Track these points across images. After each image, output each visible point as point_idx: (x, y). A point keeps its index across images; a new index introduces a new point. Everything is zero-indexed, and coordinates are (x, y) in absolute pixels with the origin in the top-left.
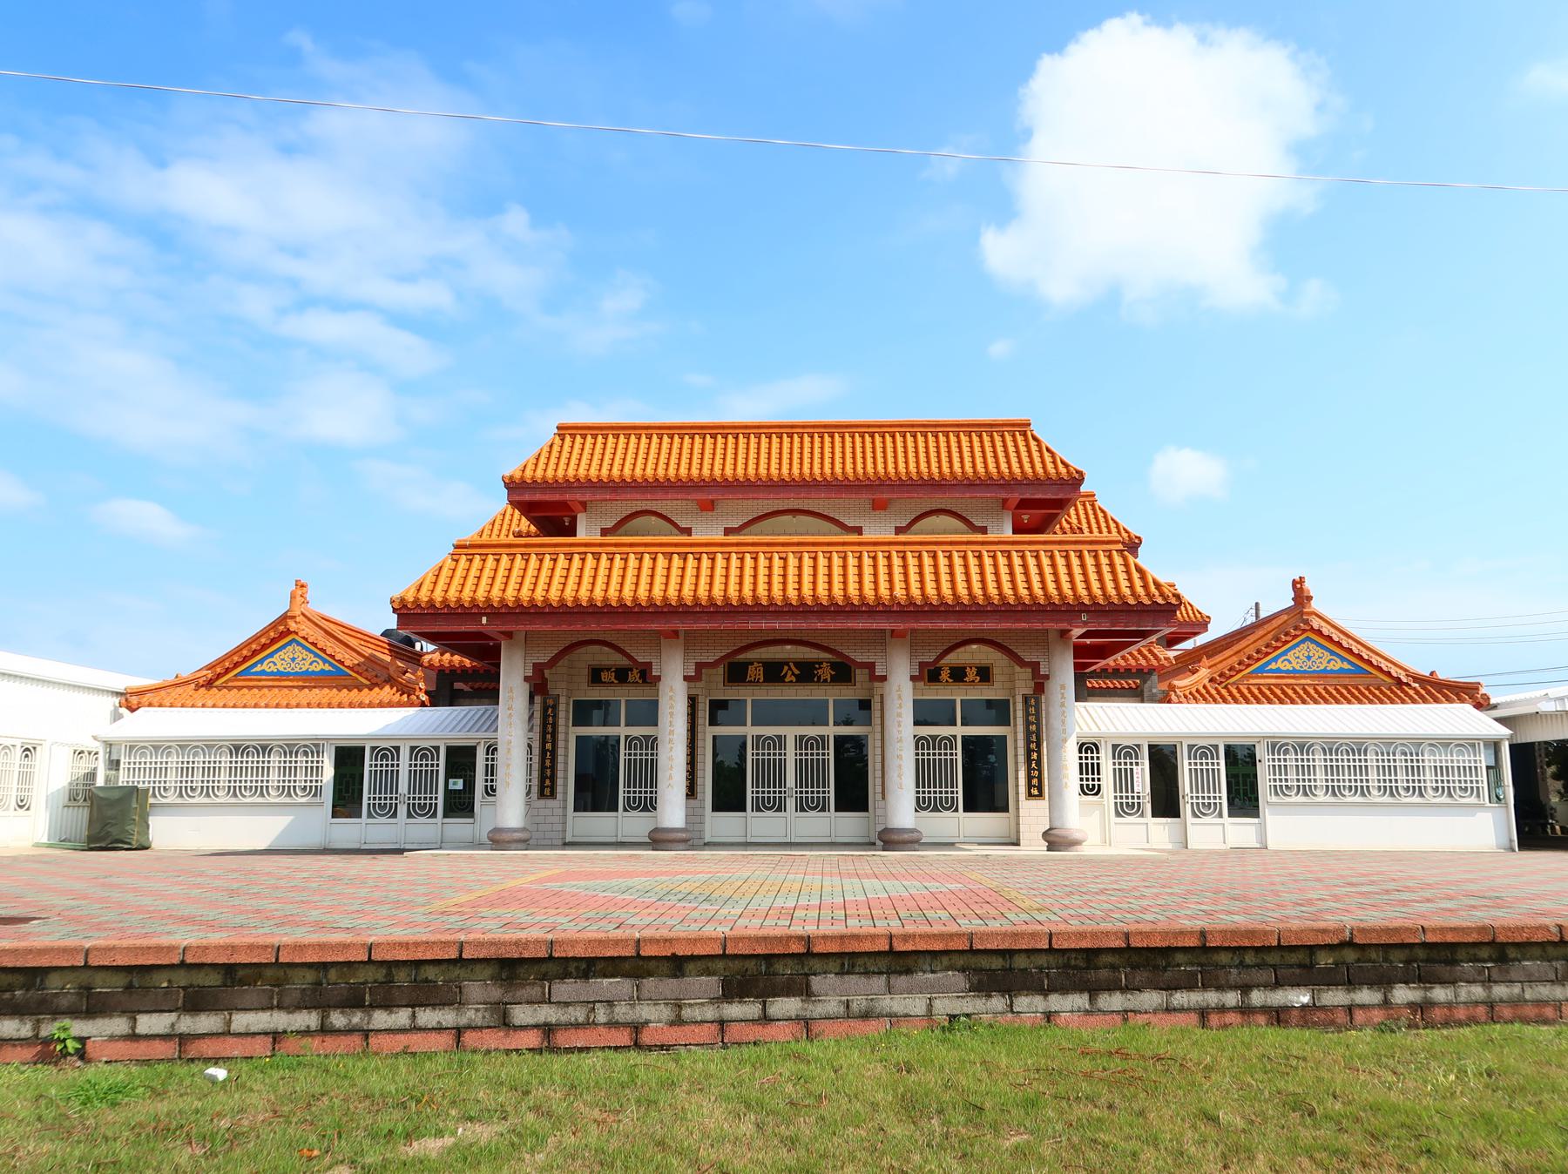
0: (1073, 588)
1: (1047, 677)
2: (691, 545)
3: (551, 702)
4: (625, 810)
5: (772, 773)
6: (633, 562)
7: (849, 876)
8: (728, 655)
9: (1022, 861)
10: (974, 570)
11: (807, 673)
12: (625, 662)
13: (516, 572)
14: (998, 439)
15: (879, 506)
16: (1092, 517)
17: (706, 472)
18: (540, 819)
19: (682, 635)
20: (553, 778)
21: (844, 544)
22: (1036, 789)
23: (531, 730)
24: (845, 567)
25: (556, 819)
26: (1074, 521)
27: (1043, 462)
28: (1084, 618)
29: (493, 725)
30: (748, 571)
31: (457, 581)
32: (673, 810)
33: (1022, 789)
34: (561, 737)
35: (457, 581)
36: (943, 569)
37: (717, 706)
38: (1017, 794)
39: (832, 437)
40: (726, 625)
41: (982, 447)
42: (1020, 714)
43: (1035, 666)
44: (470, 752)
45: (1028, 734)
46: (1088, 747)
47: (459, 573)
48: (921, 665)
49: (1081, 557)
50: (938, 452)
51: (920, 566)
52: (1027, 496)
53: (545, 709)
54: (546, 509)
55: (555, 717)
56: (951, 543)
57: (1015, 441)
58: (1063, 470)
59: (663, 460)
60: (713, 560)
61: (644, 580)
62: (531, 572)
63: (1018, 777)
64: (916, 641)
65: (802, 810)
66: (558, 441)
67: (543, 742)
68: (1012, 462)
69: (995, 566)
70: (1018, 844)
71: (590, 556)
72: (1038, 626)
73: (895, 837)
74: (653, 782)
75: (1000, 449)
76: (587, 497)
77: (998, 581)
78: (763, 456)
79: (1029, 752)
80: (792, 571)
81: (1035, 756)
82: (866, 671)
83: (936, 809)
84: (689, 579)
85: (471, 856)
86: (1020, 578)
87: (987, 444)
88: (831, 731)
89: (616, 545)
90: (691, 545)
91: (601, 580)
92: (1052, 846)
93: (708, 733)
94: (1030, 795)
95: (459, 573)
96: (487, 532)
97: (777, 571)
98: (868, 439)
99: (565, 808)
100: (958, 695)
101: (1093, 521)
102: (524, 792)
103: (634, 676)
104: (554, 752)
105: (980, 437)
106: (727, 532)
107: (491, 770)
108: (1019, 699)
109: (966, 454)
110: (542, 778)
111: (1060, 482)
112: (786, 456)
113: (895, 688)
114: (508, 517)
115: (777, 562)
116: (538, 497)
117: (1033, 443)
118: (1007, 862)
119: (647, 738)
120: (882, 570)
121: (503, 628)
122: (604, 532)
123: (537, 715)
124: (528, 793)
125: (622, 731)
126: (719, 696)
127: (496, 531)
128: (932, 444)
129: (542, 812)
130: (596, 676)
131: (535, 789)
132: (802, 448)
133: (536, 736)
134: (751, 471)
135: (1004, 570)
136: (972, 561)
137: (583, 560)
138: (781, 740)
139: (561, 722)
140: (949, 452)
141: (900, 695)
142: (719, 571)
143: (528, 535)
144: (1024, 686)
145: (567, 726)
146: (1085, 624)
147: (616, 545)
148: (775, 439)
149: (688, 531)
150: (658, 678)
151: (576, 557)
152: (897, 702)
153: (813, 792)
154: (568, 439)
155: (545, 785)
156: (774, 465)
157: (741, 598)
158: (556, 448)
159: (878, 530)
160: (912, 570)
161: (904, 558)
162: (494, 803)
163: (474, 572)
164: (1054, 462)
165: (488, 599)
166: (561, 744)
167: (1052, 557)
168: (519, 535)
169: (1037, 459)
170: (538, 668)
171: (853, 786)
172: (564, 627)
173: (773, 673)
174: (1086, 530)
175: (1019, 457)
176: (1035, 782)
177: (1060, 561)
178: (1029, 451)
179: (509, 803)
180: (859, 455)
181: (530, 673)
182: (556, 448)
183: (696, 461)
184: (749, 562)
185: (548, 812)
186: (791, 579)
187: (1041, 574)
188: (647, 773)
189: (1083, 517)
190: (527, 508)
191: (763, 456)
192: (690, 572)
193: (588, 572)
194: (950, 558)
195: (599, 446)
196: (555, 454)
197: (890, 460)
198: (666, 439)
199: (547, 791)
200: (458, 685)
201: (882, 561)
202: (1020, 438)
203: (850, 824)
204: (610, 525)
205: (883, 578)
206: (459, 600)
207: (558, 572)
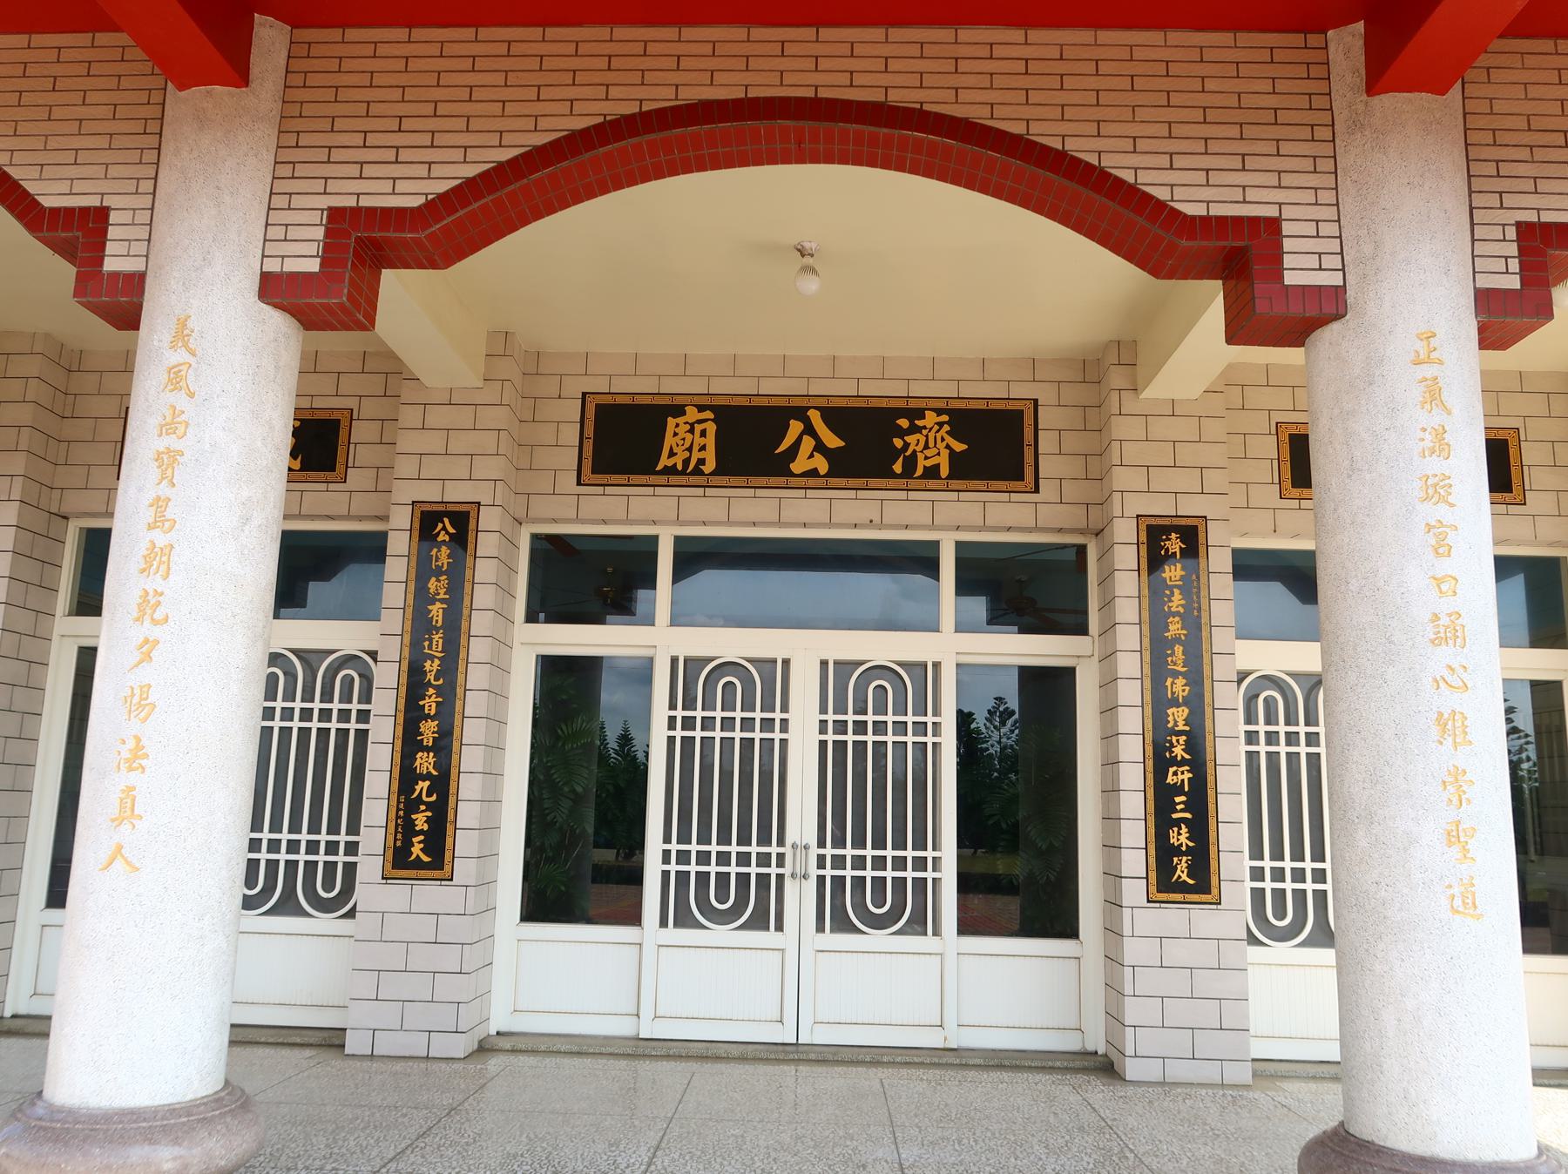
5: (738, 794)
20: (1162, 798)
33: (1135, 861)
34: (478, 649)
65: (842, 924)
108: (1125, 533)
138: (769, 680)
139: (483, 596)
145: (504, 616)
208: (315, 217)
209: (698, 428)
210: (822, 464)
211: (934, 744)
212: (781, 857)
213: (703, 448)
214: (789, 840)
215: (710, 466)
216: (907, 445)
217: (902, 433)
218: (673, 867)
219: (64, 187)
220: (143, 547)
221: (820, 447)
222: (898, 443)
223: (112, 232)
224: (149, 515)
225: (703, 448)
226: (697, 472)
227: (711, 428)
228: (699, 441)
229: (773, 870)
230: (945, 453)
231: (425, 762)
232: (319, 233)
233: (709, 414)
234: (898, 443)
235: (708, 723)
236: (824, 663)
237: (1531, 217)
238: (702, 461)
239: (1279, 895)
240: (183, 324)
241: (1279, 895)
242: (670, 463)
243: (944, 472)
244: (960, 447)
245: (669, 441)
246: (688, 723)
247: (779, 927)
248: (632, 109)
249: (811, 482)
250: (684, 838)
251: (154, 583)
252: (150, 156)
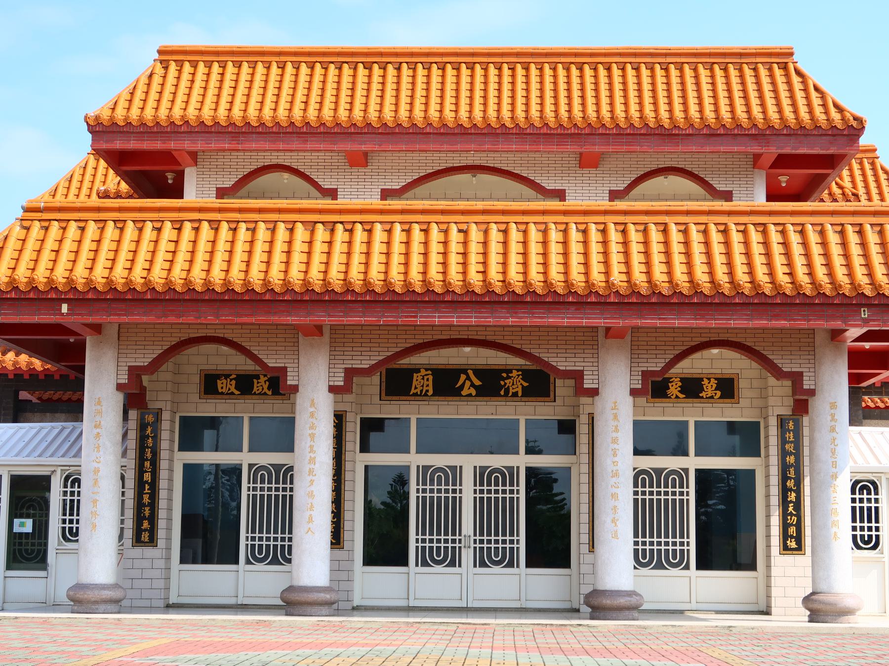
0: (851, 275)
1: (812, 393)
2: (341, 212)
3: (150, 418)
4: (248, 562)
5: (443, 517)
6: (262, 233)
7: (551, 651)
8: (388, 359)
9: (776, 635)
10: (717, 249)
11: (491, 384)
12: (247, 366)
13: (107, 245)
14: (748, 72)
15: (588, 162)
16: (871, 179)
17: (358, 114)
18: (136, 573)
19: (326, 331)
20: (153, 519)
21: (544, 213)
22: (793, 540)
23: (124, 454)
24: (545, 243)
25: (157, 573)
26: (847, 183)
27: (809, 105)
28: (865, 314)
29: (75, 447)
30: (416, 248)
31: (28, 255)
32: (312, 560)
34: (164, 465)
35: (28, 255)
36: (677, 248)
37: (371, 427)
38: (769, 546)
39: (527, 69)
40: (388, 318)
41: (728, 84)
42: (774, 441)
43: (796, 378)
44: (42, 483)
45: (784, 469)
46: (864, 487)
47: (31, 245)
48: (645, 374)
49: (861, 233)
50: (669, 91)
51: (646, 243)
52: (788, 150)
53: (142, 426)
54: (144, 161)
55: (156, 438)
56: (688, 213)
57: (772, 76)
58: (835, 115)
59: (300, 97)
60: (370, 231)
61: (278, 257)
62: (127, 245)
63: (769, 523)
64: (638, 342)
65: (483, 564)
66: (159, 70)
67: (140, 471)
68: (770, 106)
69: (746, 243)
70: (767, 613)
71: (205, 225)
72: (803, 324)
73: (607, 602)
74: (288, 525)
75: (751, 87)
76: (199, 146)
77: (828, 265)
78: (435, 93)
79: (785, 491)
80: (475, 248)
81: (792, 496)
82: (571, 382)
83: (660, 566)
84: (338, 258)
85: (45, 621)
86: (779, 260)
87: (750, 80)
88: (522, 461)
89: (241, 210)
90: (341, 212)
91: (220, 257)
92: (815, 616)
93: (358, 463)
94: (786, 548)
95: (31, 245)
96: (61, 191)
97: (455, 247)
98: (674, 72)
99: (168, 559)
100: (691, 415)
101: (872, 185)
102: (115, 533)
103: (261, 385)
104: (154, 485)
105: (725, 70)
106: (386, 194)
107: (72, 508)
108: (773, 422)
109: (706, 94)
110: (139, 518)
111: (833, 133)
112: (464, 94)
113: (609, 405)
114: (90, 171)
115: (455, 236)
116: (133, 145)
117: (796, 79)
118: (758, 636)
119: (278, 467)
120: (595, 248)
121: (90, 320)
122: (221, 193)
123: (132, 435)
124: (121, 537)
125: (245, 458)
126: (374, 413)
127: (73, 191)
128: (660, 79)
129: (137, 563)
130: (210, 385)
131: (129, 534)
132: (743, 83)
133: (131, 463)
134: (343, 114)
135: (757, 249)
136: (716, 237)
137: (197, 230)
138: (455, 472)
139: (164, 445)
140: (684, 90)
141: (617, 413)
142: (378, 247)
143: (118, 196)
144: (780, 402)
146: (866, 322)
147: (241, 210)
148: (435, 72)
149: (332, 194)
150: (295, 389)
151: (188, 226)
152: (612, 423)
153: (496, 542)
154: (173, 67)
155: (143, 528)
156: (449, 107)
157: (407, 283)
158: (157, 80)
159: (587, 193)
160: (636, 248)
161: (624, 232)
162: (76, 552)
163: (50, 244)
164: (824, 105)
165: (70, 280)
166: (163, 474)
167: (822, 233)
168: (106, 195)
169: (801, 101)
170: (135, 373)
171: (550, 539)
172: (172, 319)
173: (446, 383)
174: (863, 197)
175: (777, 98)
176: (792, 530)
177: (833, 238)
178: (791, 90)
179: (97, 551)
180: (562, 94)
181: (124, 379)
182: (157, 80)
183: (344, 99)
184: (417, 235)
185: (146, 564)
186: (474, 258)
187: (807, 255)
188: (280, 513)
189: (859, 179)
190: (119, 160)
191: (435, 93)
192: (339, 247)
193: (203, 246)
194: (685, 232)
195: (215, 77)
196: (155, 87)
197: (604, 100)
198: (304, 70)
199: (145, 536)
200: (24, 395)
201: (594, 236)
202: (778, 72)
203: (545, 583)
204: (228, 184)
205: (595, 258)
206: (31, 280)
207: (164, 245)
208: (341, 370)
209: (426, 378)
210: (473, 392)
211: (860, 507)
212: (460, 540)
213: (428, 386)
214: (463, 534)
215: (430, 393)
216: (506, 384)
217: (504, 379)
218: (420, 545)
219: (274, 361)
220: (308, 458)
221: (473, 385)
222: (502, 383)
223: (289, 374)
224: (309, 450)
226: (426, 395)
227: (431, 378)
228: (426, 383)
229: (457, 545)
230: (520, 387)
232: (343, 375)
233: (430, 372)
234: (502, 383)
235: (432, 491)
236: (475, 467)
237: (645, 369)
238: (427, 391)
239: (644, 551)
240: (313, 401)
241: (644, 551)
243: (520, 394)
244: (526, 384)
245: (415, 383)
246: (424, 491)
247: (460, 566)
248: (421, 341)
249: (469, 398)
250: (424, 534)
251: (312, 466)
252: (296, 353)
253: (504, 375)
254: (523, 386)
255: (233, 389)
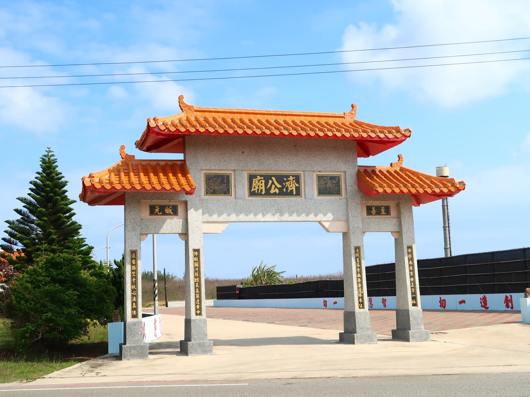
209: (260, 181)
210: (277, 191)
213: (262, 186)
217: (285, 182)
221: (276, 187)
225: (262, 186)
227: (263, 181)
230: (294, 186)
231: (359, 266)
233: (262, 178)
234: (284, 184)
242: (254, 190)
253: (285, 179)
254: (296, 186)
255: (171, 212)
